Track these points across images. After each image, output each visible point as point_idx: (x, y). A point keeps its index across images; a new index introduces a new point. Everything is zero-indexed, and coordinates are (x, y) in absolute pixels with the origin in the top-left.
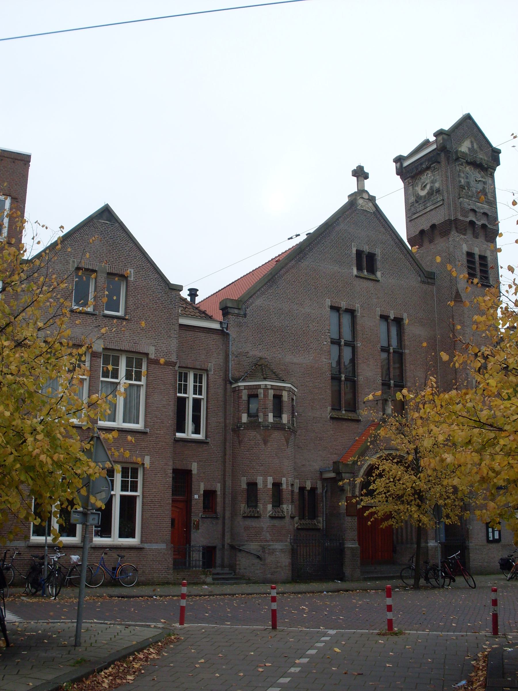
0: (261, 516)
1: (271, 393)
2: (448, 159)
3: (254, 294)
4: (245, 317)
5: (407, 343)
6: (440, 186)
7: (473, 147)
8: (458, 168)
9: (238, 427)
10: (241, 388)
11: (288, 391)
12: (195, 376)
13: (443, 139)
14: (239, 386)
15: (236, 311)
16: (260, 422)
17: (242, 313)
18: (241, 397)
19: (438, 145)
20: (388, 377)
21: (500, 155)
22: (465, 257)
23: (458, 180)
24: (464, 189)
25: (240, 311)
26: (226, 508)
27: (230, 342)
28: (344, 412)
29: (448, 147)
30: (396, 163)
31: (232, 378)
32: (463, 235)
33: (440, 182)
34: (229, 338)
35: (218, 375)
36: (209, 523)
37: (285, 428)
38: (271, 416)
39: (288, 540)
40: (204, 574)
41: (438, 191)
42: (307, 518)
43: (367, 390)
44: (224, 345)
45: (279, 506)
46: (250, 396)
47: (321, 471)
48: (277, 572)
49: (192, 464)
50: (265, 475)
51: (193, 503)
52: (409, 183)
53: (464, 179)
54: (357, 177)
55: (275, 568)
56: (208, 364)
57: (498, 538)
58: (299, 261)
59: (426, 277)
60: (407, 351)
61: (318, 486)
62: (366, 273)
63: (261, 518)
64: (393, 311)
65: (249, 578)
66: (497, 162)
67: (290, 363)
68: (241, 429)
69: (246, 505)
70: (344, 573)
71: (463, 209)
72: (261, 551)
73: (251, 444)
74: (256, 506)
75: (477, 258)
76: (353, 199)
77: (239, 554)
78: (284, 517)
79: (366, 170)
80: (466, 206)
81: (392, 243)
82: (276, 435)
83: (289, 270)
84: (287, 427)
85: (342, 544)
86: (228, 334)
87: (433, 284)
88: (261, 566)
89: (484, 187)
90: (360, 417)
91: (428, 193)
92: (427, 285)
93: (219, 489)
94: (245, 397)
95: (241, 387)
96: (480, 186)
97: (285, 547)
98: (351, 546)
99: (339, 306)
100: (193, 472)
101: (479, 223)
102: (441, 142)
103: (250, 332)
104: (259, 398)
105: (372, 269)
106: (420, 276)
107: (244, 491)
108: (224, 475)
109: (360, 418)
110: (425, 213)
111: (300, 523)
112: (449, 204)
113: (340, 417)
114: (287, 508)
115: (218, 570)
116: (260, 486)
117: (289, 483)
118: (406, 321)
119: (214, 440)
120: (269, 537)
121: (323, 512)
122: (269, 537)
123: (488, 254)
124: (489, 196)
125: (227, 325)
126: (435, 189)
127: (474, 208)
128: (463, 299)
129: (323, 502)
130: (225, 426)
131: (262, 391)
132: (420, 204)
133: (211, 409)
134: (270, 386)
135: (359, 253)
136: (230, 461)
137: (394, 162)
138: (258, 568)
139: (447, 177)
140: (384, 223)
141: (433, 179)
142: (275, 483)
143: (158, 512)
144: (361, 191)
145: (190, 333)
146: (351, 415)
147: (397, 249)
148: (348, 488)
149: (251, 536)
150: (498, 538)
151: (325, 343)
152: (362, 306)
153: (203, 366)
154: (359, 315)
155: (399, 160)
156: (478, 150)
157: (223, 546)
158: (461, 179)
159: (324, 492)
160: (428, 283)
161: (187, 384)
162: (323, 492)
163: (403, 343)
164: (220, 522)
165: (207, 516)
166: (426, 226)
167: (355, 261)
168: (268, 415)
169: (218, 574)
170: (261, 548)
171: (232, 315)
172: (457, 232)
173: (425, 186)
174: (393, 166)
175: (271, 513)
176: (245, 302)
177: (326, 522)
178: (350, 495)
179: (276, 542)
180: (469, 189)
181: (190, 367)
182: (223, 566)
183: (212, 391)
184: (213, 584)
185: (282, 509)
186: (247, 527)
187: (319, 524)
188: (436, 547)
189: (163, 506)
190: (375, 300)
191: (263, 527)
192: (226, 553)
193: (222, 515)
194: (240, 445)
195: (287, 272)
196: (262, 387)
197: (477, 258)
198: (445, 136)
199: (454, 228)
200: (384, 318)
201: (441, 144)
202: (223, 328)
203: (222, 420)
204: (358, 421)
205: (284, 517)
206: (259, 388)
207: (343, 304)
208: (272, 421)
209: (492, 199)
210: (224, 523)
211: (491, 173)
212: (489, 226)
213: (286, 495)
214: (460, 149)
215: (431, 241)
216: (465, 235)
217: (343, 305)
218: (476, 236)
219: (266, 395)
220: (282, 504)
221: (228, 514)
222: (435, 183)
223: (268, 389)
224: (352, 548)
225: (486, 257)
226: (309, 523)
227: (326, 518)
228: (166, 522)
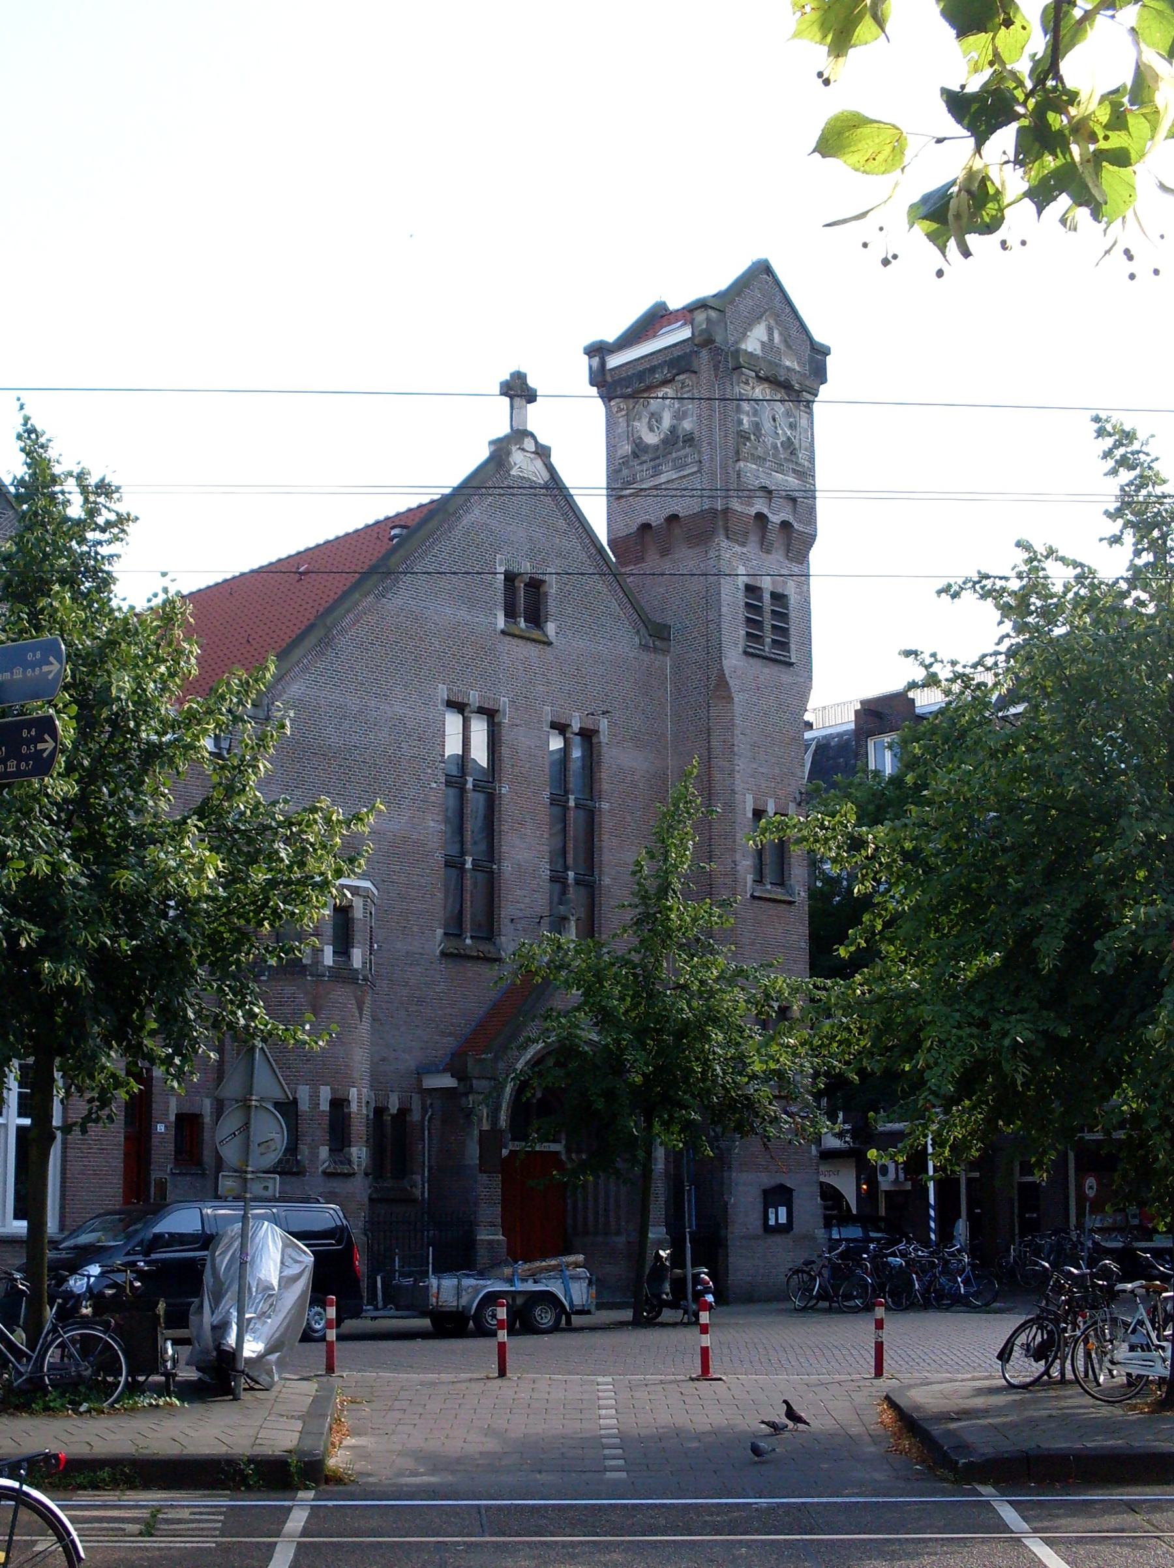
0: (306, 1171)
5: (605, 786)
7: (771, 339)
11: (364, 897)
13: (708, 320)
20: (561, 861)
22: (741, 595)
24: (749, 439)
28: (468, 941)
29: (718, 338)
30: (590, 358)
32: (740, 545)
33: (695, 418)
37: (358, 979)
41: (689, 440)
43: (519, 892)
45: (342, 1150)
50: (315, 1085)
51: (155, 1141)
54: (511, 398)
57: (785, 1222)
58: (383, 596)
59: (650, 636)
60: (605, 806)
61: (414, 1107)
62: (523, 624)
63: (305, 1176)
66: (819, 373)
75: (767, 597)
76: (500, 452)
78: (354, 1174)
79: (531, 382)
82: (342, 995)
83: (361, 617)
84: (361, 977)
87: (666, 651)
90: (503, 954)
92: (652, 656)
93: (209, 1110)
98: (487, 1238)
99: (466, 701)
101: (775, 519)
105: (536, 618)
114: (359, 1153)
116: (304, 1106)
118: (604, 738)
123: (790, 589)
124: (802, 455)
126: (680, 433)
129: (424, 1141)
132: (645, 462)
137: (585, 353)
140: (567, 508)
141: (679, 409)
143: (96, 1162)
144: (519, 434)
146: (485, 947)
150: (785, 1222)
151: (434, 785)
155: (597, 351)
156: (782, 347)
158: (742, 417)
160: (655, 650)
163: (596, 786)
166: (654, 513)
167: (500, 597)
168: (322, 951)
172: (728, 538)
174: (582, 366)
175: (326, 1164)
180: (758, 438)
187: (414, 1190)
189: (106, 1149)
190: (541, 688)
197: (767, 597)
199: (721, 531)
205: (354, 1174)
208: (331, 964)
209: (806, 463)
212: (796, 525)
213: (359, 1127)
214: (743, 347)
216: (743, 544)
218: (765, 546)
224: (490, 1242)
225: (786, 596)
228: (111, 1183)
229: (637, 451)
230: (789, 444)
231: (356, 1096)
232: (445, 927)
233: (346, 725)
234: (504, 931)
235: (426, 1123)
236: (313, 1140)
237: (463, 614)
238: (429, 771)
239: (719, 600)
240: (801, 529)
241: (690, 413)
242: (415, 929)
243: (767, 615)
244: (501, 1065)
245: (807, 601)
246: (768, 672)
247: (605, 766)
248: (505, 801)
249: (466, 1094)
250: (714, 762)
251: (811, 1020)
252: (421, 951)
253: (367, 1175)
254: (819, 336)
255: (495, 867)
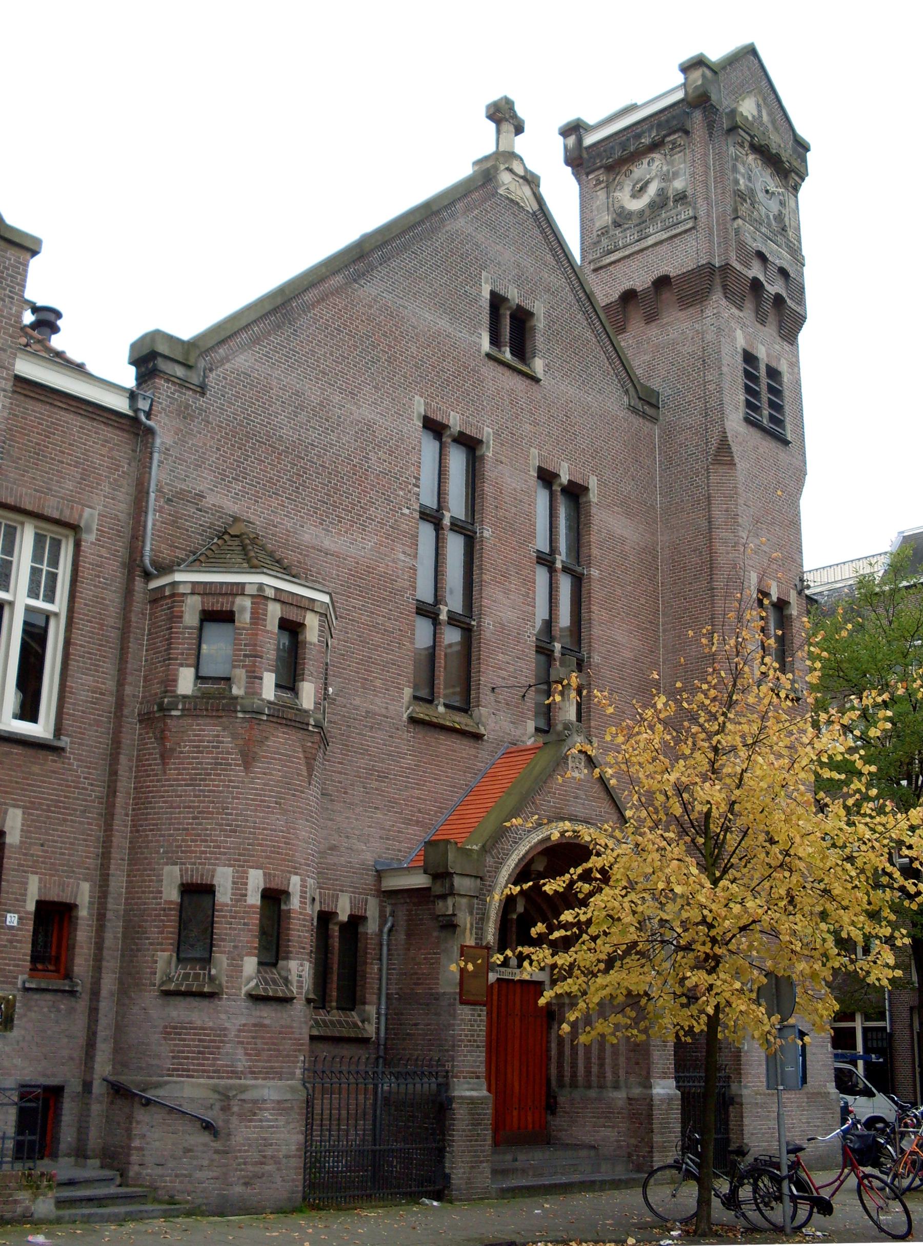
1: (274, 611)
2: (710, 127)
3: (232, 335)
4: (203, 394)
5: (595, 552)
6: (687, 187)
8: (732, 150)
9: (161, 708)
10: (182, 589)
11: (321, 614)
12: (39, 540)
14: (174, 584)
15: (180, 371)
16: (236, 698)
17: (195, 379)
18: (181, 617)
19: (690, 91)
21: (808, 154)
22: (739, 359)
23: (731, 178)
25: (189, 373)
26: (104, 964)
27: (156, 456)
28: (441, 709)
31: (153, 563)
33: (687, 176)
34: (153, 443)
35: (107, 548)
36: (45, 1010)
37: (308, 724)
38: (269, 680)
39: (298, 1072)
40: (31, 1187)
41: (681, 198)
42: (334, 1004)
43: (500, 657)
44: (133, 464)
45: (275, 965)
46: (210, 617)
47: (379, 868)
48: (263, 1175)
49: (6, 813)
50: (241, 864)
52: (599, 182)
53: (744, 178)
55: (256, 1163)
56: (82, 510)
59: (640, 398)
60: (595, 573)
61: (368, 914)
63: (220, 999)
64: (566, 465)
65: (172, 1197)
67: (313, 548)
68: (174, 713)
69: (175, 955)
70: (447, 1177)
71: (741, 245)
72: (218, 1106)
73: (201, 763)
74: (207, 961)
77: (141, 1115)
79: (521, 111)
80: (749, 241)
81: (571, 298)
85: (445, 1086)
86: (150, 431)
87: (654, 420)
88: (216, 1157)
89: (780, 213)
90: (482, 728)
91: (652, 205)
92: (641, 420)
94: (190, 616)
95: (181, 586)
96: (773, 206)
97: (288, 1096)
98: (468, 1093)
99: (445, 421)
100: (9, 840)
102: (700, 82)
103: (213, 438)
104: (237, 624)
105: (521, 349)
106: (627, 392)
107: (170, 909)
108: (105, 856)
109: (482, 730)
110: (642, 250)
111: (316, 1021)
112: (711, 229)
113: (435, 720)
115: (64, 1168)
116: (224, 896)
117: (308, 895)
118: (593, 496)
119: (80, 744)
120: (242, 1063)
121: (380, 989)
122: (242, 1063)
123: (783, 367)
125: (151, 405)
126: (671, 193)
127: (764, 250)
128: (737, 460)
129: (380, 959)
130: (120, 704)
131: (247, 603)
133: (81, 646)
134: (273, 591)
135: (497, 301)
136: (127, 815)
138: (206, 1163)
139: (707, 166)
142: (269, 889)
145: (39, 407)
147: (580, 316)
148: (465, 919)
149: (187, 1058)
151: (406, 511)
152: (497, 434)
153: (67, 512)
154: (490, 455)
155: (574, 129)
157: (87, 1086)
159: (386, 930)
160: (644, 415)
161: (11, 562)
162: (381, 931)
163: (584, 550)
164: (82, 1005)
165: (43, 986)
168: (261, 678)
169: (71, 1183)
170: (216, 1096)
171: (168, 381)
172: (726, 297)
173: (643, 189)
175: (253, 984)
176: (208, 351)
177: (387, 1019)
178: (470, 941)
179: (264, 1079)
181: (29, 507)
182: (80, 1153)
183: (86, 592)
184: (58, 1221)
185: (284, 973)
186: (176, 1028)
188: (670, 1099)
191: (225, 1029)
192: (96, 1108)
193: (89, 986)
194: (164, 764)
195: (323, 299)
196: (249, 590)
198: (708, 73)
200: (546, 477)
201: (696, 87)
202: (136, 410)
203: (111, 685)
204: (478, 737)
206: (237, 594)
207: (455, 418)
210: (93, 1012)
211: (796, 185)
215: (651, 318)
216: (740, 308)
217: (455, 421)
219: (258, 617)
220: (287, 958)
221: (108, 983)
222: (674, 179)
223: (267, 598)
224: (472, 1101)
226: (339, 1022)
227: (387, 1008)
229: (618, 220)
230: (779, 218)
231: (298, 888)
232: (416, 687)
233: (303, 417)
234: (483, 702)
235: (385, 937)
236: (235, 947)
237: (443, 324)
238: (401, 493)
239: (719, 360)
240: (793, 306)
241: (682, 172)
242: (378, 683)
243: (764, 388)
244: (489, 860)
245: (797, 383)
246: (767, 446)
247: (594, 528)
248: (488, 545)
249: (444, 897)
250: (716, 533)
251: (694, 882)
252: (384, 711)
253: (309, 1001)
254: (802, 131)
255: (473, 623)
